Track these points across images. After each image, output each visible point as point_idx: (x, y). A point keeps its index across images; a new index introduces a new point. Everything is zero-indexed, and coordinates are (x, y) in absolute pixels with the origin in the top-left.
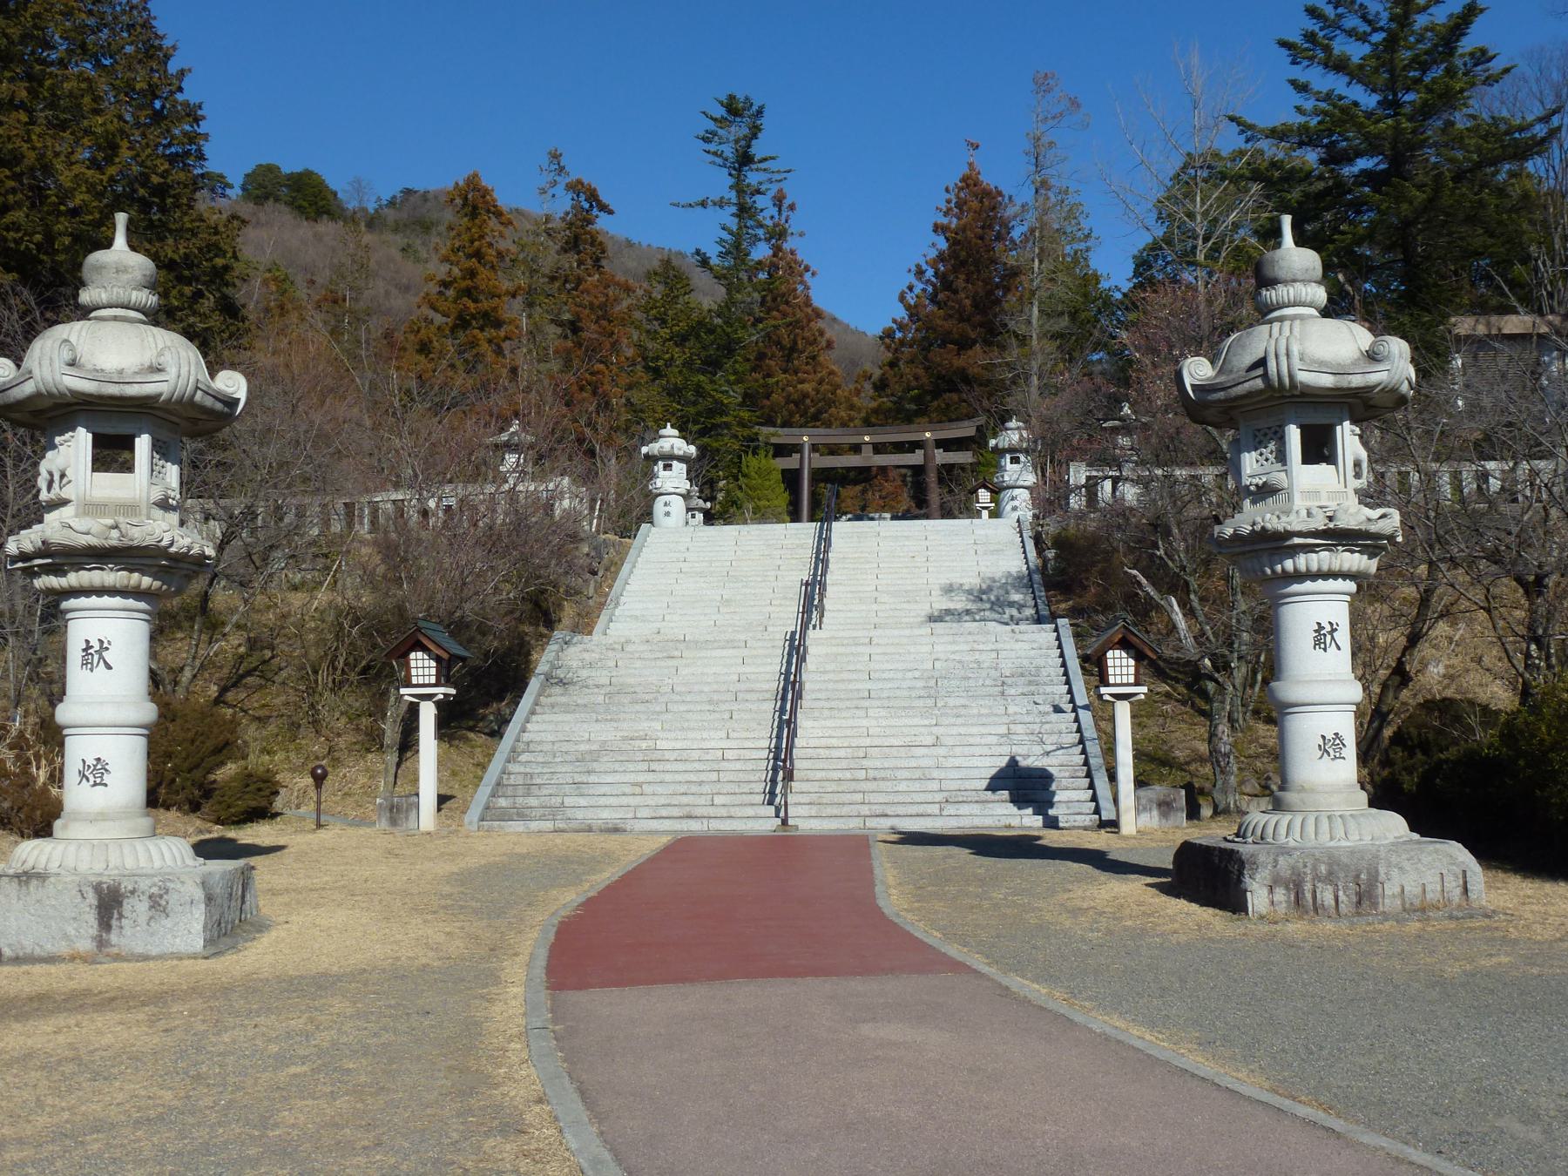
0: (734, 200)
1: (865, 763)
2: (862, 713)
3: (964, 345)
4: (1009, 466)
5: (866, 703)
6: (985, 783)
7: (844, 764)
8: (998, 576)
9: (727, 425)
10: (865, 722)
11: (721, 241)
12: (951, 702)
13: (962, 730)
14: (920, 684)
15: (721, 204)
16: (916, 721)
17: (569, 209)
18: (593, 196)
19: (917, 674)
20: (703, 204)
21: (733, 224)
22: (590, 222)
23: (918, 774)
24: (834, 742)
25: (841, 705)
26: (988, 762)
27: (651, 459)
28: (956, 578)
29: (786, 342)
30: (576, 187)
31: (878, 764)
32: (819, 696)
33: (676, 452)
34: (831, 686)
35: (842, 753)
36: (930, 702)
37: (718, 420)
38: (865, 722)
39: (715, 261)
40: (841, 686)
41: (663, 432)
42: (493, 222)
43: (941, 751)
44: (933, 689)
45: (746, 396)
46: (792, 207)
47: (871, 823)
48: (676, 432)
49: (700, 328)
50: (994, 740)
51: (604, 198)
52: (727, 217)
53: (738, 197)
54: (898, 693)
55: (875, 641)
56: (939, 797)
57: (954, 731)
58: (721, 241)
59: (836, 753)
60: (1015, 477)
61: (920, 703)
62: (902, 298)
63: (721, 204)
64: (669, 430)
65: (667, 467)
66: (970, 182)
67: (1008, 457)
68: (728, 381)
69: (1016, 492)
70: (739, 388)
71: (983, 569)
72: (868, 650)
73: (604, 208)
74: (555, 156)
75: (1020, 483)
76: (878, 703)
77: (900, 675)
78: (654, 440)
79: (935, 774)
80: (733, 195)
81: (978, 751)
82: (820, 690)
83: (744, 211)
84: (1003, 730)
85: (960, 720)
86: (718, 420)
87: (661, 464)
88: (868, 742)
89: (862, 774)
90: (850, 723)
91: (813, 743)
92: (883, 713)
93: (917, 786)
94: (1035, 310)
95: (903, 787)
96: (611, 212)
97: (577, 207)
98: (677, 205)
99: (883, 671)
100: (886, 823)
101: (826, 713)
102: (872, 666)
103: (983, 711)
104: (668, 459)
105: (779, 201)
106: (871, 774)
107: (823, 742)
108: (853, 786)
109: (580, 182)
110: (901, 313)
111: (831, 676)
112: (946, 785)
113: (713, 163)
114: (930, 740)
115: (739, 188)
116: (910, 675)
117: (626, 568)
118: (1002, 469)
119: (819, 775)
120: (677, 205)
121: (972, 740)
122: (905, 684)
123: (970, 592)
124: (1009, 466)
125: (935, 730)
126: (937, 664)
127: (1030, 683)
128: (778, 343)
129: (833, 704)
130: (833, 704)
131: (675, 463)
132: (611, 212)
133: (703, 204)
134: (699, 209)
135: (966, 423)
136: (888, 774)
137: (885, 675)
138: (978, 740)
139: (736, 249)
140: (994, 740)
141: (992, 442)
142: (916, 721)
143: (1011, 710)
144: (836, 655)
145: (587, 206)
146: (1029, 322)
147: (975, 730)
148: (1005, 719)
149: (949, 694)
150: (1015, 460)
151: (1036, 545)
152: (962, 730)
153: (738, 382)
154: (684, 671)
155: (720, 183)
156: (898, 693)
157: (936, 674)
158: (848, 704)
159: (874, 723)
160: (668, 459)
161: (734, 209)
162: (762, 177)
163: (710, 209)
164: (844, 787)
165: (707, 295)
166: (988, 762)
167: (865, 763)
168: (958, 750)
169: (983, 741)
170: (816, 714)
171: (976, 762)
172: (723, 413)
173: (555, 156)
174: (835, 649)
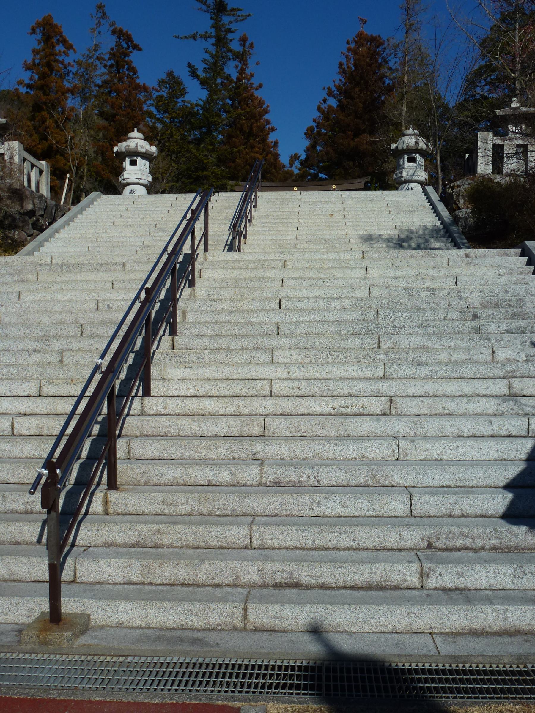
0: (213, 34)
1: (263, 449)
2: (264, 357)
3: (357, 133)
4: (406, 165)
5: (272, 342)
6: (502, 501)
7: (221, 450)
8: (415, 228)
9: (206, 177)
10: (267, 372)
11: (205, 61)
12: (403, 341)
13: (431, 387)
14: (353, 316)
15: (205, 37)
16: (352, 371)
17: (113, 46)
18: (128, 39)
19: (347, 303)
20: (194, 37)
21: (213, 49)
22: (126, 55)
23: (362, 476)
24: (210, 405)
25: (233, 344)
26: (492, 450)
27: (121, 156)
28: (375, 230)
29: (246, 128)
30: (120, 34)
31: (285, 450)
32: (204, 330)
33: (139, 149)
34: (223, 317)
35: (221, 427)
36: (370, 342)
37: (200, 173)
38: (267, 372)
39: (200, 73)
40: (237, 318)
41: (131, 135)
42: (60, 48)
43: (400, 427)
44: (375, 322)
45: (219, 160)
46: (252, 46)
47: (262, 615)
48: (141, 135)
49: (188, 115)
50: (491, 405)
51: (136, 41)
52: (209, 44)
53: (216, 31)
54: (321, 328)
55: (290, 264)
56: (412, 537)
57: (417, 388)
58: (205, 61)
59: (210, 427)
60: (411, 172)
61: (354, 343)
62: (319, 109)
63: (205, 37)
64: (135, 134)
65: (133, 163)
66: (361, 39)
67: (406, 157)
68: (208, 150)
69: (412, 185)
70: (215, 154)
71: (398, 224)
72: (281, 274)
73: (137, 47)
74: (100, 7)
75: (415, 178)
76: (290, 342)
77: (322, 304)
78: (125, 140)
79: (398, 476)
80: (213, 31)
81: (468, 426)
82: (206, 323)
83: (221, 41)
84: (501, 387)
85: (423, 371)
86: (200, 173)
87: (128, 160)
88: (269, 405)
89: (251, 474)
90: (244, 372)
91: (173, 406)
92: (297, 357)
93: (359, 506)
94: (405, 108)
95: (332, 506)
96: (140, 49)
97: (118, 45)
98: (177, 37)
99: (300, 300)
100: (296, 615)
101: (208, 356)
102: (284, 292)
103: (456, 356)
104: (134, 155)
105: (243, 40)
106: (272, 473)
107: (192, 405)
108: (230, 502)
109: (121, 31)
110: (317, 115)
111: (226, 305)
112: (427, 504)
113: (201, 9)
114: (377, 405)
115: (217, 26)
116: (336, 304)
117: (61, 221)
118: (400, 167)
119: (169, 474)
120: (177, 37)
121: (450, 406)
122: (331, 316)
123: (389, 240)
124: (406, 165)
125: (384, 387)
126: (375, 293)
127: (514, 316)
128: (241, 130)
129: (221, 343)
130: (221, 343)
131: (139, 160)
132: (140, 49)
133: (194, 37)
134: (191, 40)
135: (358, 180)
136: (304, 474)
137: (303, 305)
138: (461, 406)
139: (215, 67)
140: (491, 405)
141: (393, 146)
142: (352, 371)
143: (501, 355)
144: (236, 280)
145: (125, 46)
146: (400, 114)
147: (452, 388)
148: (497, 371)
149: (398, 329)
150: (411, 160)
151: (446, 206)
152: (431, 387)
153: (213, 150)
154: (29, 298)
155: (204, 23)
156: (321, 328)
157: (375, 304)
158: (244, 342)
159: (282, 372)
160: (134, 155)
161: (213, 41)
162: (232, 18)
163: (199, 40)
164: (216, 503)
165: (195, 94)
166: (492, 450)
167: (263, 449)
168: (432, 426)
169: (472, 408)
170: (193, 357)
171: (470, 450)
172: (204, 169)
173: (100, 7)
174: (236, 274)
